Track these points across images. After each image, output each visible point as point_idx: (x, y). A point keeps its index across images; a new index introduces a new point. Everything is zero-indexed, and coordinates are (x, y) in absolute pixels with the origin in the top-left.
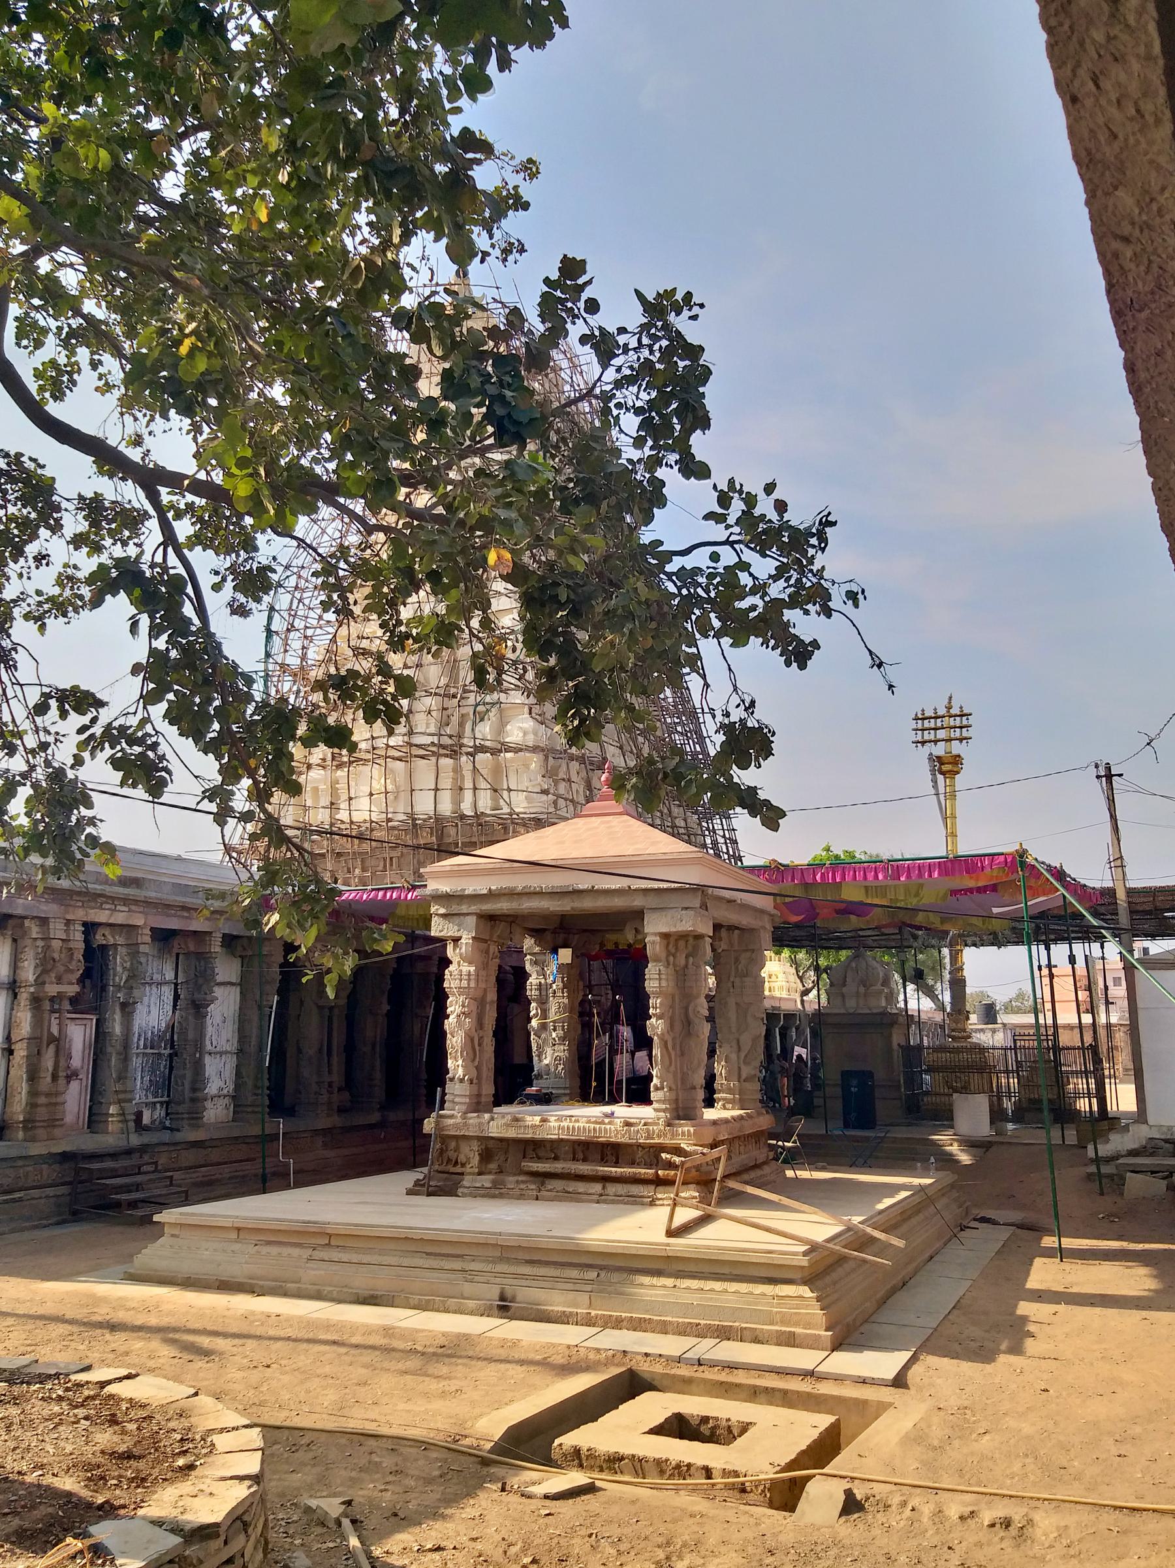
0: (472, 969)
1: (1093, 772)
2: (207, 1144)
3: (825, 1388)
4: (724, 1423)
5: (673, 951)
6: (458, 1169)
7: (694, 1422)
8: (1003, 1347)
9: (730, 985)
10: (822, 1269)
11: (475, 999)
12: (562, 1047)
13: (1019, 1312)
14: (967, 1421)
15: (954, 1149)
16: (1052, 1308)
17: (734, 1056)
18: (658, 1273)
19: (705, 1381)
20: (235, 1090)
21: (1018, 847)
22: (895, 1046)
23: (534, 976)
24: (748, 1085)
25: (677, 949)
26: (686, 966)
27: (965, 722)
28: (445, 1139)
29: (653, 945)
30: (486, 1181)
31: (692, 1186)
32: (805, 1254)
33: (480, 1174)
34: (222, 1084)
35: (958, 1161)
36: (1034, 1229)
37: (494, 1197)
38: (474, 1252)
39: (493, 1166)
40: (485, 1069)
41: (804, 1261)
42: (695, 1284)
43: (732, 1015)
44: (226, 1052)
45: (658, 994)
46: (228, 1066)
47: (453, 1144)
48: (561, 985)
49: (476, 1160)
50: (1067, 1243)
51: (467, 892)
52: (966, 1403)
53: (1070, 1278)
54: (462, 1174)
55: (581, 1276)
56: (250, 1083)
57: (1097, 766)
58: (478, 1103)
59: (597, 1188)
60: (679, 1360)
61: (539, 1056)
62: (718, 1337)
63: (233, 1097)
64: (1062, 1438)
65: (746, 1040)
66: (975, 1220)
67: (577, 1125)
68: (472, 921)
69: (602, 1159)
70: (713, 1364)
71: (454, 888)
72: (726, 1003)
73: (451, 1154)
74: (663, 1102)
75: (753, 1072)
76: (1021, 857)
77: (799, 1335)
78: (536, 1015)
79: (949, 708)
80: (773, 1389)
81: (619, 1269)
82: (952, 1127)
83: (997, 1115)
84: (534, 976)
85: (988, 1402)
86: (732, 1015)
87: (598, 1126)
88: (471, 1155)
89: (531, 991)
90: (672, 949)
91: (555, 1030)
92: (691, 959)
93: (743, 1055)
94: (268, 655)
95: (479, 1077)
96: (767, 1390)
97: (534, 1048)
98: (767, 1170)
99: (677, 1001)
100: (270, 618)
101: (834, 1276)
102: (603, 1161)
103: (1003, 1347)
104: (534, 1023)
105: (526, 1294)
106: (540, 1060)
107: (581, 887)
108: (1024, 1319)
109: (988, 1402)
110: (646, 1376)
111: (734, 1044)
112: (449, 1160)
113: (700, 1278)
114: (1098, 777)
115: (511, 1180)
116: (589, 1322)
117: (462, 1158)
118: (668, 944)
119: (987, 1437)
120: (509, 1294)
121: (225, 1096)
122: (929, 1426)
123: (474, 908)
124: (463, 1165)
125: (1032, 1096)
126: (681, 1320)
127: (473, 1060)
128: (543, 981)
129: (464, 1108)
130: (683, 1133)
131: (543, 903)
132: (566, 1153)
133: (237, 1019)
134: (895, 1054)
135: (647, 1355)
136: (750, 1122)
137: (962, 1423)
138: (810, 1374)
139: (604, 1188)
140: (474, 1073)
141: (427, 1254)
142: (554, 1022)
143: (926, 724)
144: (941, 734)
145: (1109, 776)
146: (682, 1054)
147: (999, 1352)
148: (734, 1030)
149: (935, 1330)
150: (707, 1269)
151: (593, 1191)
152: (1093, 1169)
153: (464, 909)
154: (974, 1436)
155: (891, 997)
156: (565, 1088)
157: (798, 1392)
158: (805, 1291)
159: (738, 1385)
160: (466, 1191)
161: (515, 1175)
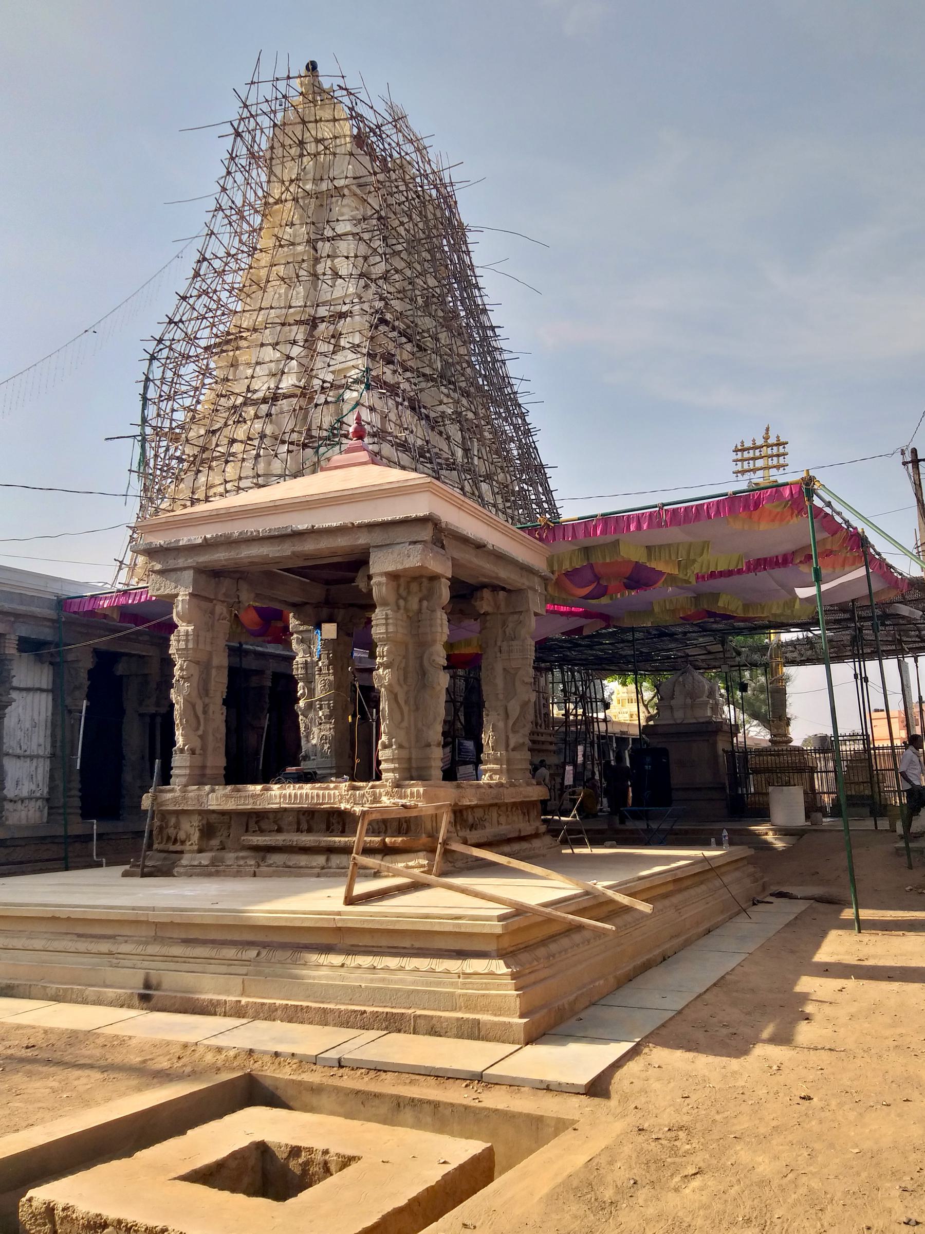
0: (190, 628)
1: (899, 458)
2: (8, 843)
3: (495, 1100)
4: (319, 1157)
5: (404, 594)
6: (178, 847)
7: (282, 1155)
8: (765, 1034)
9: (497, 649)
10: (525, 940)
11: (198, 663)
12: (328, 726)
13: (798, 989)
14: (674, 1151)
15: (770, 837)
16: (838, 983)
17: (501, 724)
18: (327, 949)
19: (337, 1090)
20: (49, 793)
21: (804, 475)
22: (720, 752)
23: (301, 654)
24: (517, 755)
25: (409, 593)
26: (420, 611)
27: (781, 450)
28: (165, 815)
29: (379, 588)
30: (205, 859)
31: (421, 854)
32: (501, 918)
33: (200, 851)
34: (33, 787)
35: (775, 849)
36: (835, 902)
37: (210, 875)
38: (126, 931)
39: (215, 842)
40: (210, 738)
41: (497, 928)
42: (366, 961)
43: (500, 682)
44: (38, 757)
45: (386, 641)
46: (40, 770)
47: (173, 821)
48: (326, 662)
49: (196, 837)
50: (866, 914)
51: (181, 543)
52: (685, 1120)
53: (865, 951)
54: (182, 852)
55: (139, 951)
56: (61, 786)
57: (903, 453)
58: (203, 775)
59: (321, 860)
60: (315, 1060)
61: (307, 737)
62: (386, 1028)
63: (48, 800)
64: (815, 1184)
65: (514, 708)
66: (772, 895)
67: (299, 792)
68: (189, 575)
69: (328, 829)
70: (357, 1066)
71: (168, 540)
72: (493, 668)
73: (171, 831)
74: (392, 761)
75: (521, 741)
76: (807, 484)
77: (485, 1023)
78: (303, 695)
79: (766, 438)
80: (420, 1100)
81: (283, 946)
82: (770, 821)
83: (812, 807)
84: (301, 654)
85: (718, 1117)
86: (500, 682)
87: (321, 792)
88: (190, 829)
89: (298, 671)
90: (403, 592)
91: (321, 708)
92: (425, 603)
93: (511, 723)
94: (144, 420)
95: (204, 748)
96: (414, 1103)
97: (302, 729)
98: (536, 843)
99: (411, 647)
100: (146, 388)
101: (553, 947)
102: (329, 830)
103: (765, 1034)
104: (302, 703)
105: (174, 979)
106: (308, 741)
107: (300, 527)
108: (804, 998)
109: (718, 1117)
110: (268, 1083)
111: (502, 712)
112: (169, 838)
113: (403, 955)
114: (905, 463)
115: (230, 857)
116: (238, 1012)
117: (182, 835)
118: (399, 586)
119: (696, 1183)
120: (154, 981)
121: (37, 799)
122: (611, 1163)
123: (190, 562)
124: (183, 842)
125: (849, 793)
126: (343, 1007)
127: (197, 729)
128: (309, 659)
129: (184, 780)
130: (412, 794)
131: (261, 550)
132: (290, 824)
133: (49, 724)
134: (721, 760)
135: (277, 1054)
136: (512, 790)
137: (665, 1155)
138: (476, 1078)
139: (328, 860)
140: (197, 744)
141: (79, 935)
142: (320, 700)
143: (746, 455)
144: (760, 463)
145: (916, 462)
146: (417, 709)
147: (755, 1040)
148: (501, 696)
149: (680, 1012)
150: (384, 942)
151: (314, 864)
152: (902, 844)
153: (181, 562)
154: (677, 1179)
155: (716, 708)
156: (331, 768)
157: (452, 1105)
158: (499, 967)
159: (377, 1096)
160: (182, 870)
161: (236, 851)
